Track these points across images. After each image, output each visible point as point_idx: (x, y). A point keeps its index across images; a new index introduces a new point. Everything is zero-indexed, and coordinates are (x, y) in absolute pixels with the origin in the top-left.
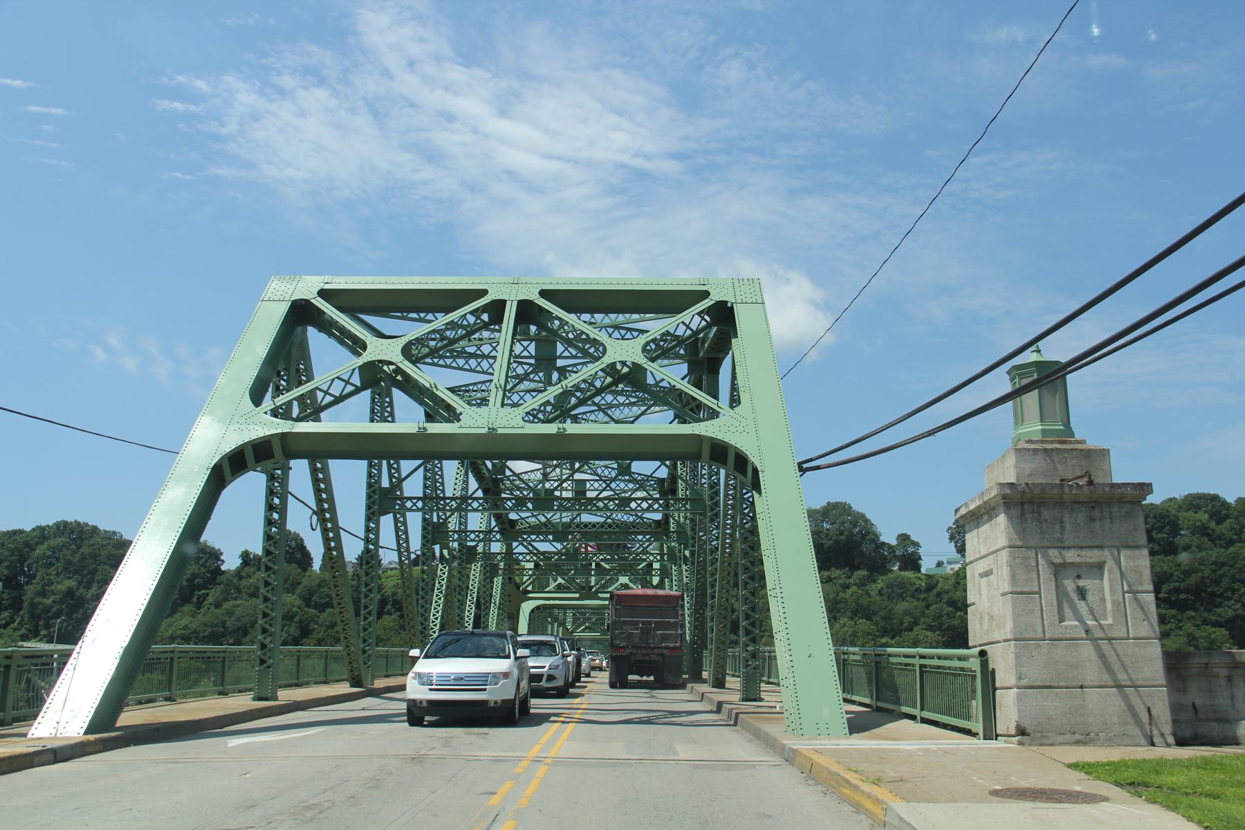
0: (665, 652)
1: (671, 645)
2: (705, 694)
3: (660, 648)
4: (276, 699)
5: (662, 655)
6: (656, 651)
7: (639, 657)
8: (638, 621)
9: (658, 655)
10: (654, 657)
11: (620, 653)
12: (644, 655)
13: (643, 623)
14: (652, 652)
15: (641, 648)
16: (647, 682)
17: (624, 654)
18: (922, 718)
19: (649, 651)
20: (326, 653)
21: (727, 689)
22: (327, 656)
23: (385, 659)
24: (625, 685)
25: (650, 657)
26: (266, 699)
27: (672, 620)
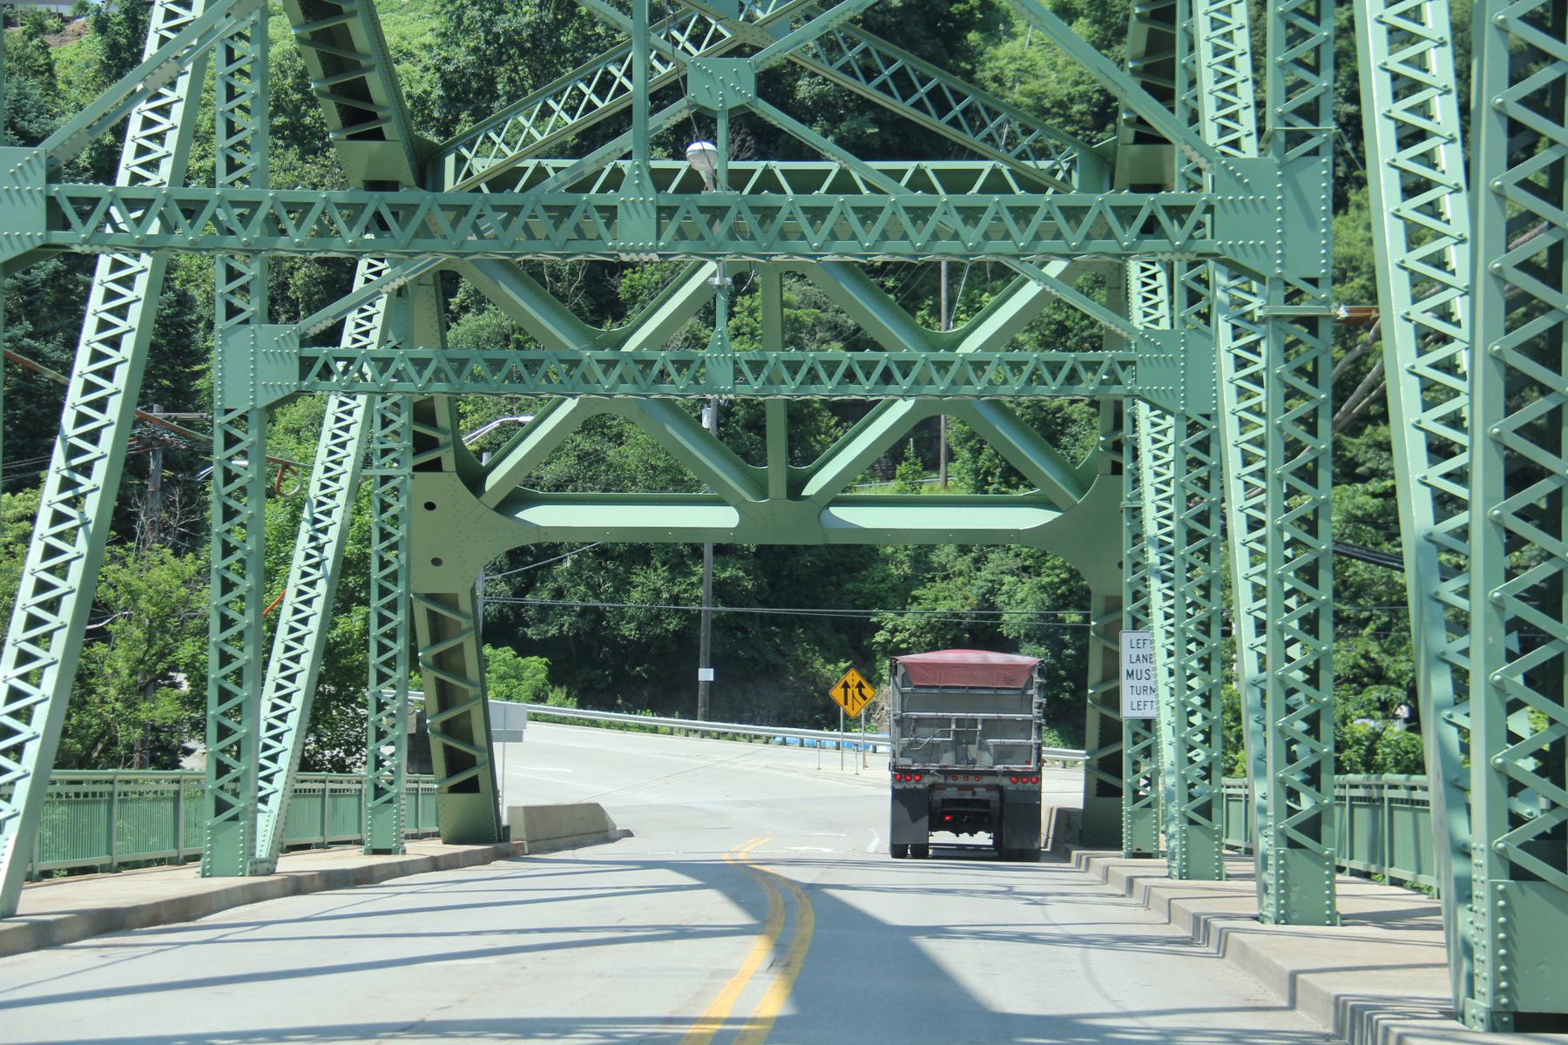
0: (1005, 782)
1: (1017, 768)
2: (1301, 976)
3: (994, 773)
4: (271, 872)
5: (1000, 788)
6: (986, 780)
7: (951, 793)
8: (949, 720)
9: (989, 788)
10: (981, 794)
11: (911, 785)
12: (961, 788)
13: (959, 721)
14: (979, 783)
15: (955, 774)
16: (977, 847)
17: (920, 786)
18: (1351, 870)
19: (972, 781)
20: (175, 787)
21: (1228, 877)
22: (177, 793)
23: (170, 805)
24: (921, 852)
25: (974, 794)
26: (388, 852)
27: (1019, 716)
